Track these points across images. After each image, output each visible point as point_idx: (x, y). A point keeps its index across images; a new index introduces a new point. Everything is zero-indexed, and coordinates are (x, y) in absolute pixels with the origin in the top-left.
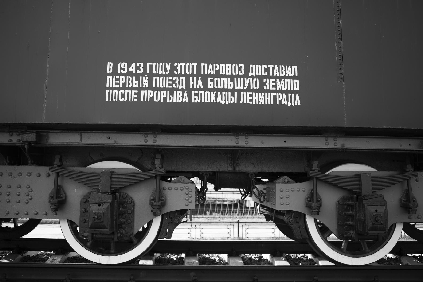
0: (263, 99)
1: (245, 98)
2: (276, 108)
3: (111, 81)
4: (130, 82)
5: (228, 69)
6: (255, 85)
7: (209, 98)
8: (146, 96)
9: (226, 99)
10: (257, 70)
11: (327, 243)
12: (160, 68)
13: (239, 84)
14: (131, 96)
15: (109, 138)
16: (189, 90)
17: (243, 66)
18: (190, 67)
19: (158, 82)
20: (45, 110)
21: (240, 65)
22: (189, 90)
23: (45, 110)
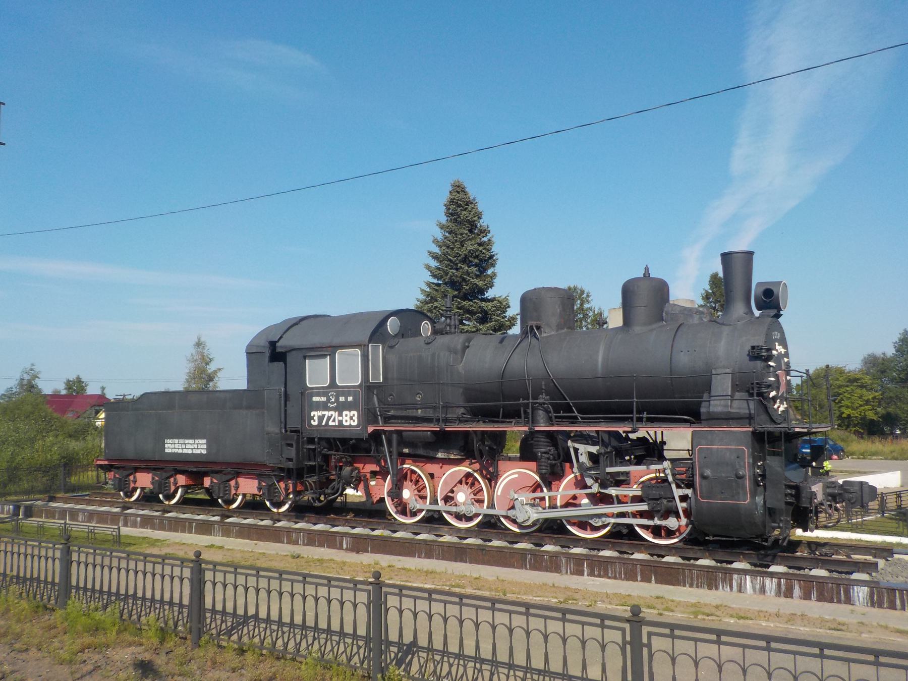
12: (176, 441)
21: (353, 413)
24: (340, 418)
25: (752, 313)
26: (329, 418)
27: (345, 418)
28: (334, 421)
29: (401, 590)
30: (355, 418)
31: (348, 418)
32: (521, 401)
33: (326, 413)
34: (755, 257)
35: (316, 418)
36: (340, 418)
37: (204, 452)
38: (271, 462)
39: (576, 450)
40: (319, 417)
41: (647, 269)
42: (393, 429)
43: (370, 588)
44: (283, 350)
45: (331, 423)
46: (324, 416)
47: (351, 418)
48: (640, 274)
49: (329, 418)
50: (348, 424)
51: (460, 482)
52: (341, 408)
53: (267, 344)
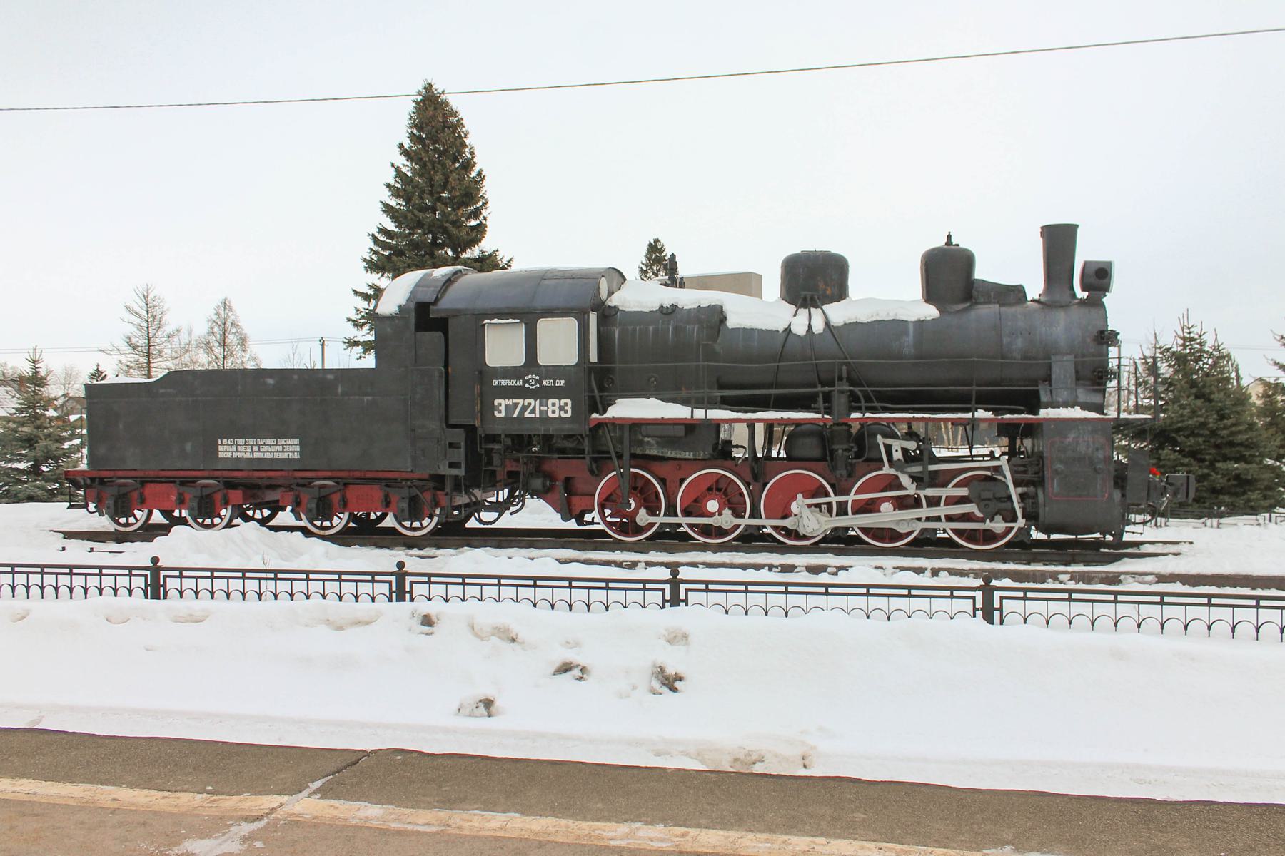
0: (285, 456)
1: (276, 456)
2: (289, 460)
3: (220, 448)
4: (228, 448)
5: (269, 441)
6: (280, 448)
7: (261, 455)
8: (235, 455)
9: (268, 456)
10: (281, 441)
11: (480, 305)
12: (241, 441)
13: (273, 449)
14: (229, 455)
15: (670, 682)
16: (253, 452)
17: (569, 402)
18: (252, 441)
19: (240, 448)
20: (679, 412)
21: (563, 401)
22: (253, 452)
23: (679, 412)
24: (544, 408)
25: (1074, 295)
26: (524, 408)
27: (551, 408)
28: (533, 411)
29: (181, 572)
30: (568, 408)
31: (556, 408)
32: (819, 389)
33: (521, 401)
34: (1079, 230)
35: (502, 408)
36: (544, 408)
37: (297, 456)
38: (403, 464)
39: (888, 449)
40: (507, 406)
41: (949, 237)
42: (1023, 416)
43: (148, 573)
44: (443, 315)
45: (527, 415)
46: (517, 405)
47: (561, 408)
48: (941, 242)
49: (524, 408)
50: (556, 415)
51: (710, 489)
52: (543, 394)
53: (412, 306)
